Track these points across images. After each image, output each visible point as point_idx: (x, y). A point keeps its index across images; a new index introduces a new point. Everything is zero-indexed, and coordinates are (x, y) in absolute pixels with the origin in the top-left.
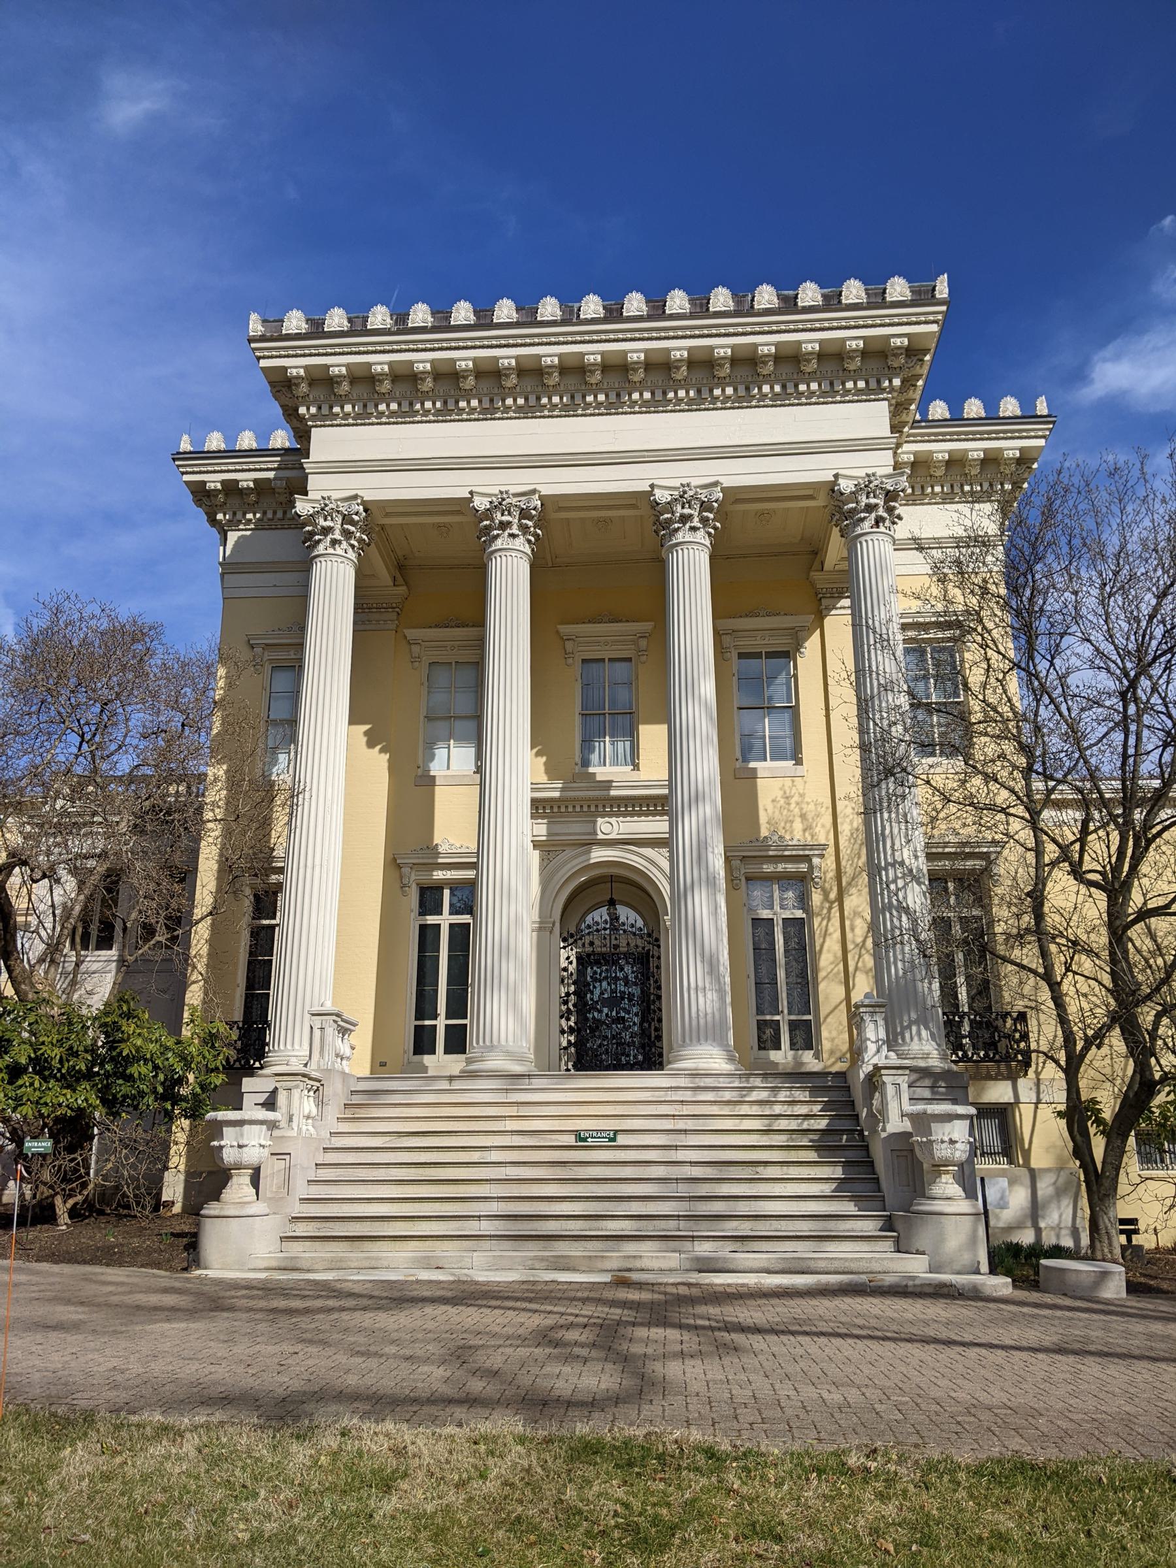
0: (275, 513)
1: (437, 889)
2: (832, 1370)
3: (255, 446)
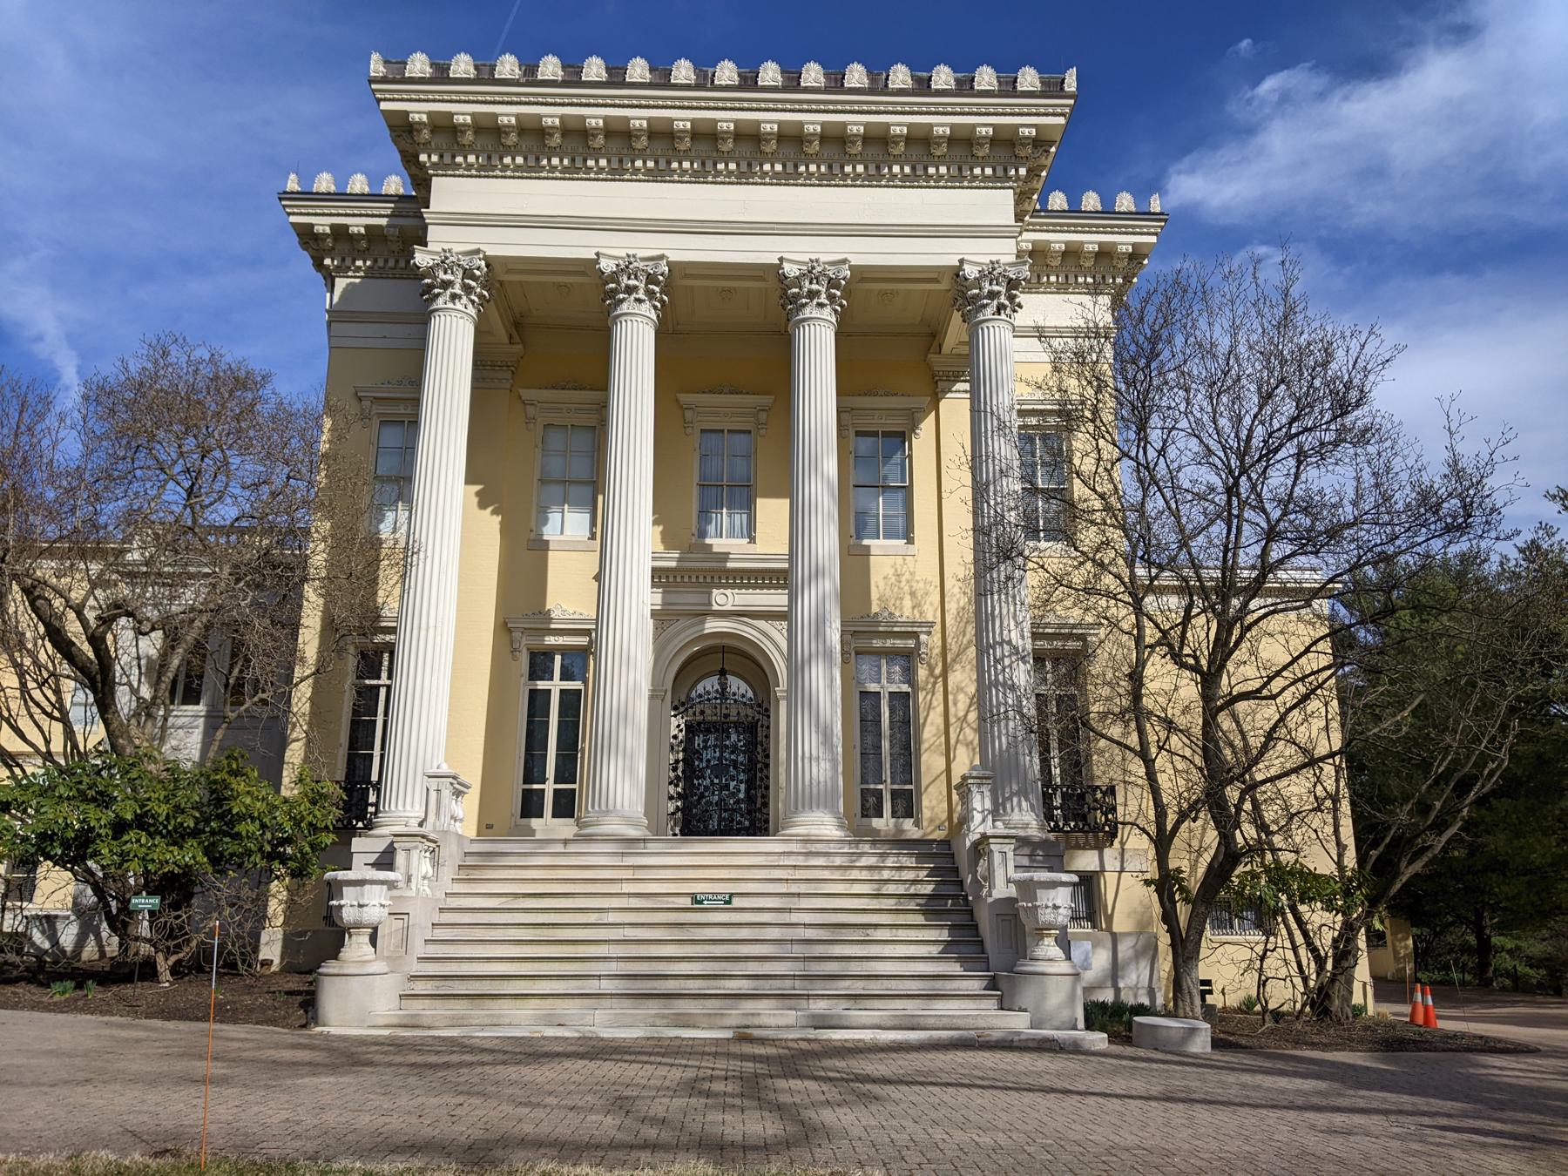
0: (386, 261)
1: (548, 654)
3: (367, 190)
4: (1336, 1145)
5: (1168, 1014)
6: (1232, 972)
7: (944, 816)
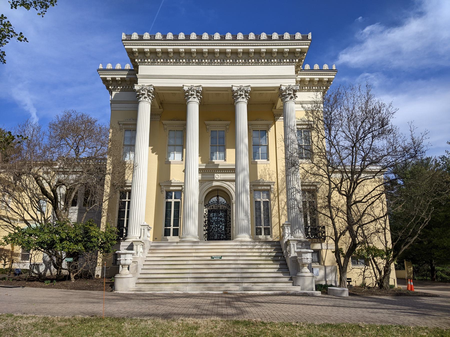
0: (126, 87)
1: (171, 192)
2: (283, 309)
4: (372, 315)
5: (339, 287)
6: (356, 275)
7: (279, 234)
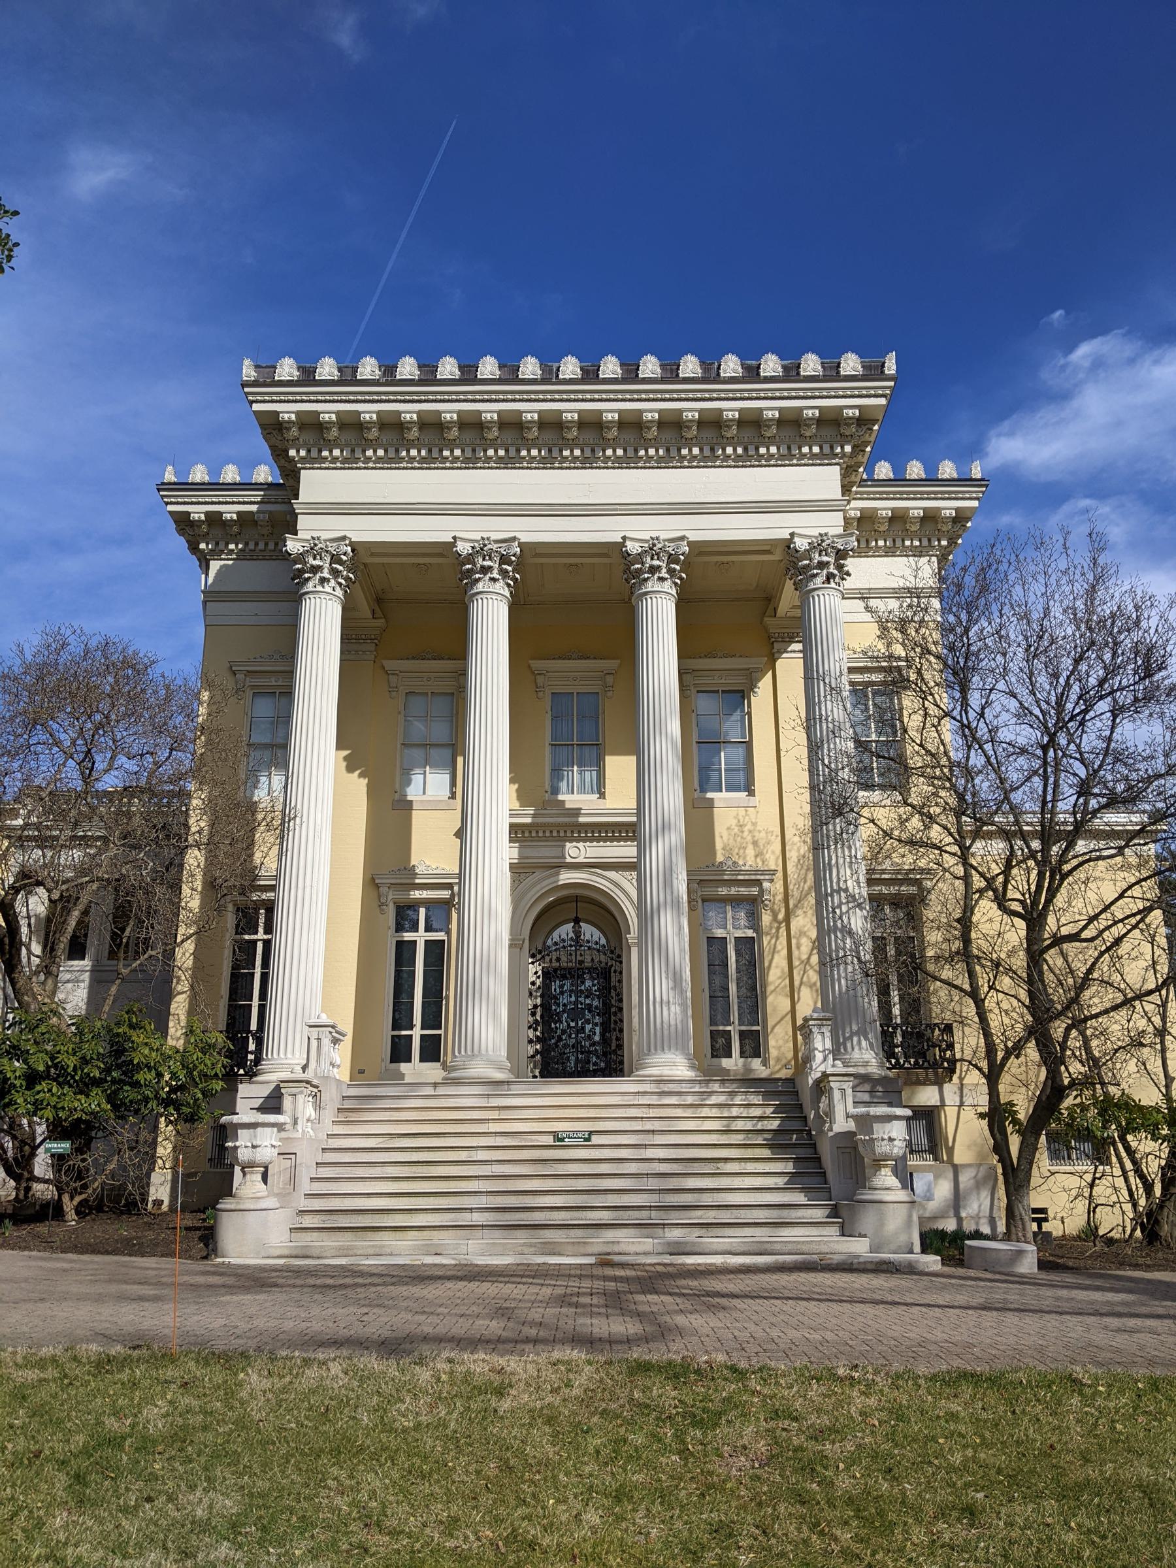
0: (257, 544)
1: (414, 906)
2: (805, 1320)
4: (1121, 1340)
7: (790, 1055)
